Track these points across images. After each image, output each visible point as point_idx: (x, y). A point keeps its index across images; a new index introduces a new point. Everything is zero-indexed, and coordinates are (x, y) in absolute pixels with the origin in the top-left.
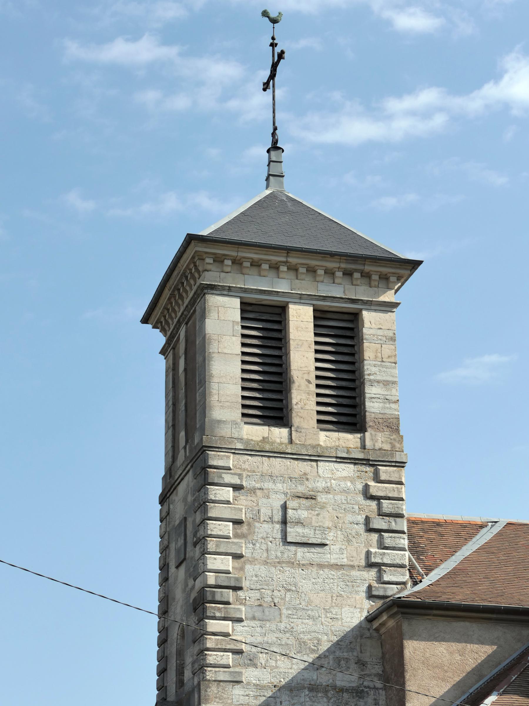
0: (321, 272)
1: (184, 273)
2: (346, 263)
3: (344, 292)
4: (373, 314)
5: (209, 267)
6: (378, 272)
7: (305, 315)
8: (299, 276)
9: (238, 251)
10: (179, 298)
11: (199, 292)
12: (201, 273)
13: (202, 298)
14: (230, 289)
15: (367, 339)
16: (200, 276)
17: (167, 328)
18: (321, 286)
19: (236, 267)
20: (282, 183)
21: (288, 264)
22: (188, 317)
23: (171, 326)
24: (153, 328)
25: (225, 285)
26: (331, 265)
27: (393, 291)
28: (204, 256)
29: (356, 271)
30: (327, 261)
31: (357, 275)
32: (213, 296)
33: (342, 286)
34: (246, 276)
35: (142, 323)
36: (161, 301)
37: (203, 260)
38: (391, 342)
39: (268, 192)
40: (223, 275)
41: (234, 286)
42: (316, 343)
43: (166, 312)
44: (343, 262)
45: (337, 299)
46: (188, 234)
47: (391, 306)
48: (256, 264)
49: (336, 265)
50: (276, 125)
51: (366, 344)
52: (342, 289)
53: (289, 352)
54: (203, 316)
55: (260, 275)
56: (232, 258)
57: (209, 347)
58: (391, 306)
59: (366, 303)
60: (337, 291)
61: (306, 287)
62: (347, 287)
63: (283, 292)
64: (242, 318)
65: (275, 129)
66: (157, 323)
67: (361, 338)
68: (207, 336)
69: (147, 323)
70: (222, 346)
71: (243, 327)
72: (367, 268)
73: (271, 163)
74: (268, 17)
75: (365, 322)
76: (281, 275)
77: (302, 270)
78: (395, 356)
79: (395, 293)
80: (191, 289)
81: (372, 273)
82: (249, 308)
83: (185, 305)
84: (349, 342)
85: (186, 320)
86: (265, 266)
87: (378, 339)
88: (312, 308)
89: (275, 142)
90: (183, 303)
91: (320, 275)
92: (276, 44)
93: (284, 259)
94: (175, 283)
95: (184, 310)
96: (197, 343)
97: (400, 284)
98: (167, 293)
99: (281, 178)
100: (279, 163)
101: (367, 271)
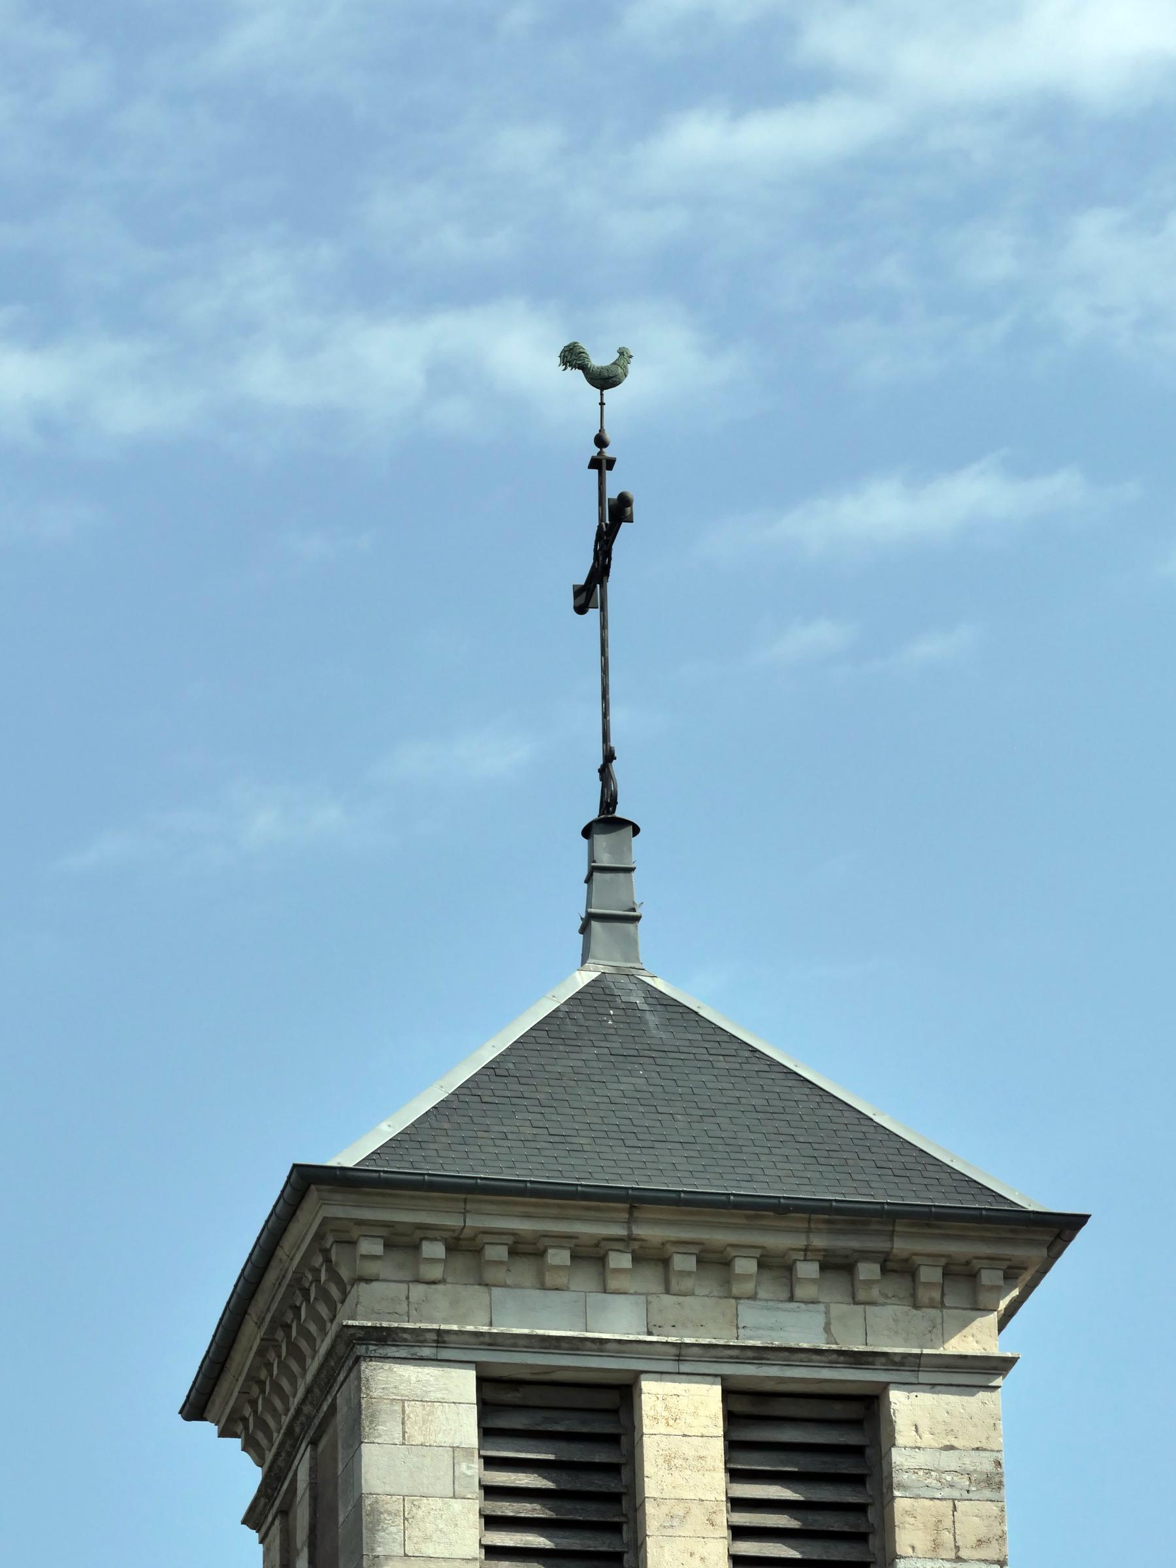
0: (745, 1266)
1: (298, 1279)
2: (830, 1232)
3: (827, 1328)
4: (926, 1399)
5: (371, 1268)
6: (943, 1256)
7: (695, 1414)
8: (674, 1281)
9: (465, 1213)
10: (298, 1333)
11: (341, 1349)
12: (348, 1287)
13: (351, 1370)
14: (441, 1338)
15: (904, 1487)
16: (345, 1295)
17: (264, 1442)
18: (749, 1314)
19: (461, 1262)
20: (632, 943)
21: (635, 1245)
22: (316, 1422)
23: (275, 1435)
24: (223, 1434)
25: (424, 1326)
26: (778, 1241)
27: (993, 1318)
28: (355, 1232)
29: (866, 1255)
30: (765, 1229)
31: (867, 1271)
32: (387, 1366)
33: (821, 1307)
34: (495, 1291)
35: (188, 1418)
36: (237, 1357)
37: (353, 1243)
38: (987, 1493)
39: (583, 978)
40: (418, 1291)
41: (455, 1327)
42: (736, 1504)
43: (255, 1390)
44: (819, 1231)
45: (802, 1356)
46: (295, 1166)
47: (986, 1370)
48: (527, 1250)
49: (799, 1241)
50: (613, 743)
51: (902, 1504)
52: (821, 1320)
53: (644, 1542)
54: (355, 1437)
55: (543, 1287)
56: (446, 1235)
57: (374, 1541)
58: (986, 1370)
59: (902, 1364)
60: (800, 1328)
61: (700, 1320)
62: (837, 1309)
63: (619, 1341)
64: (487, 1432)
65: (609, 756)
66: (231, 1419)
67: (886, 1482)
68: (367, 1502)
69: (201, 1418)
70: (416, 1533)
71: (490, 1463)
72: (902, 1246)
73: (596, 875)
74: (584, 368)
75: (897, 1428)
76: (613, 1284)
77: (683, 1262)
78: (1002, 1537)
79: (1002, 1324)
80: (323, 1331)
81: (918, 1260)
82: (509, 1397)
83: (309, 1377)
84: (847, 1495)
85: (311, 1433)
86: (559, 1257)
87: (943, 1485)
88: (717, 1390)
89: (609, 802)
90: (315, 1352)
91: (745, 1277)
92: (611, 463)
93: (620, 1231)
94: (274, 1307)
95: (303, 1401)
96: (341, 1519)
97: (1015, 1293)
98: (251, 1335)
99: (630, 927)
100: (621, 875)
101: (905, 1255)
